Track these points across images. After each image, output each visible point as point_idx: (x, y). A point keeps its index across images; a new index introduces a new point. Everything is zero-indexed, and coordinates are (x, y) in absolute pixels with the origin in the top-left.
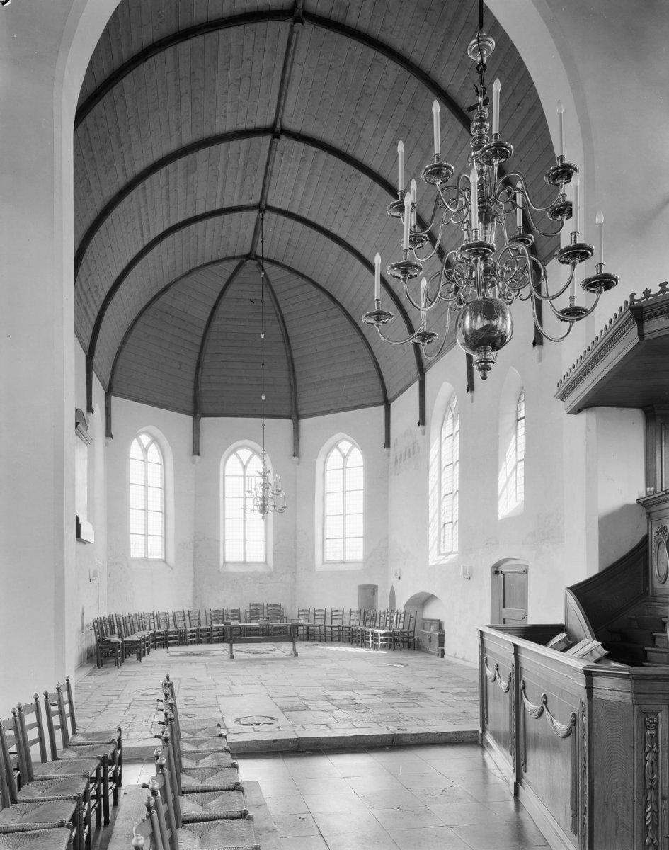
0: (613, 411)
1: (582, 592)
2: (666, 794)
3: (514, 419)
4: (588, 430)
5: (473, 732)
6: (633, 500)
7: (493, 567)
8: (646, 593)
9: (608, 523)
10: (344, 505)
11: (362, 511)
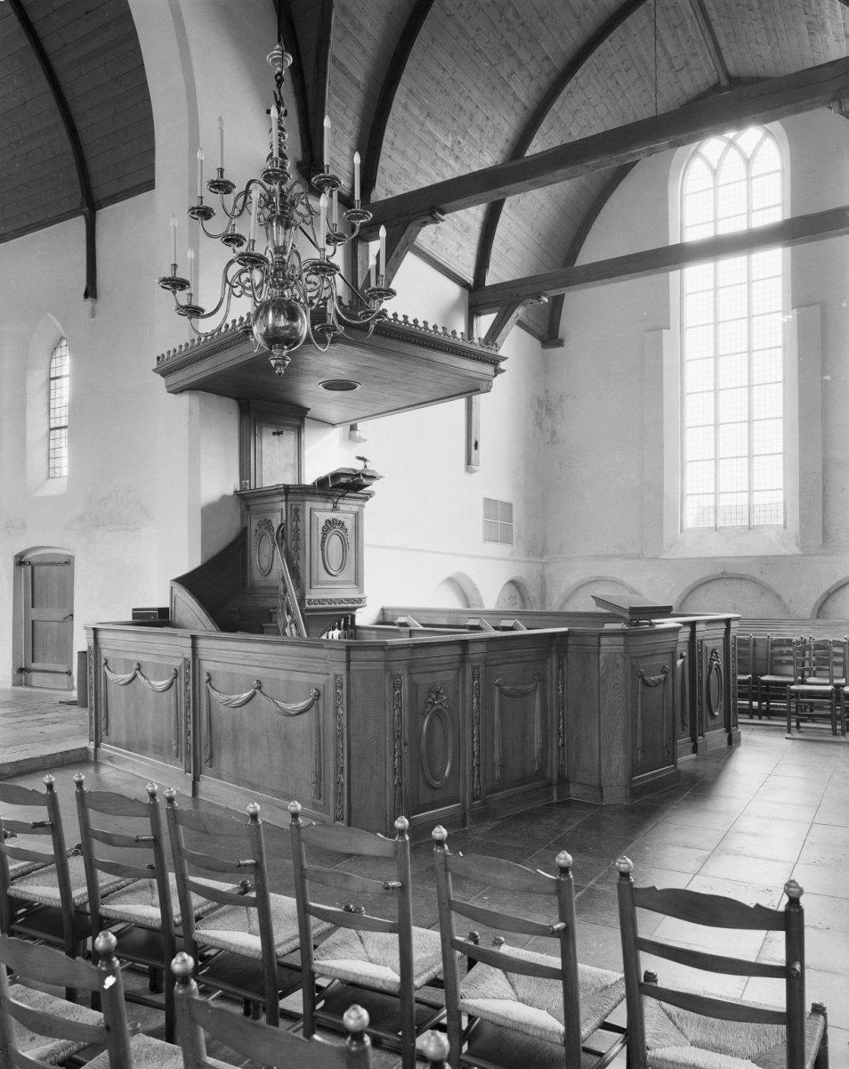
0: (213, 398)
1: (188, 582)
2: (407, 741)
3: (45, 378)
4: (191, 413)
5: (82, 749)
6: (230, 492)
7: (16, 556)
8: (244, 584)
9: (210, 513)
10: (750, 374)
11: (780, 378)
